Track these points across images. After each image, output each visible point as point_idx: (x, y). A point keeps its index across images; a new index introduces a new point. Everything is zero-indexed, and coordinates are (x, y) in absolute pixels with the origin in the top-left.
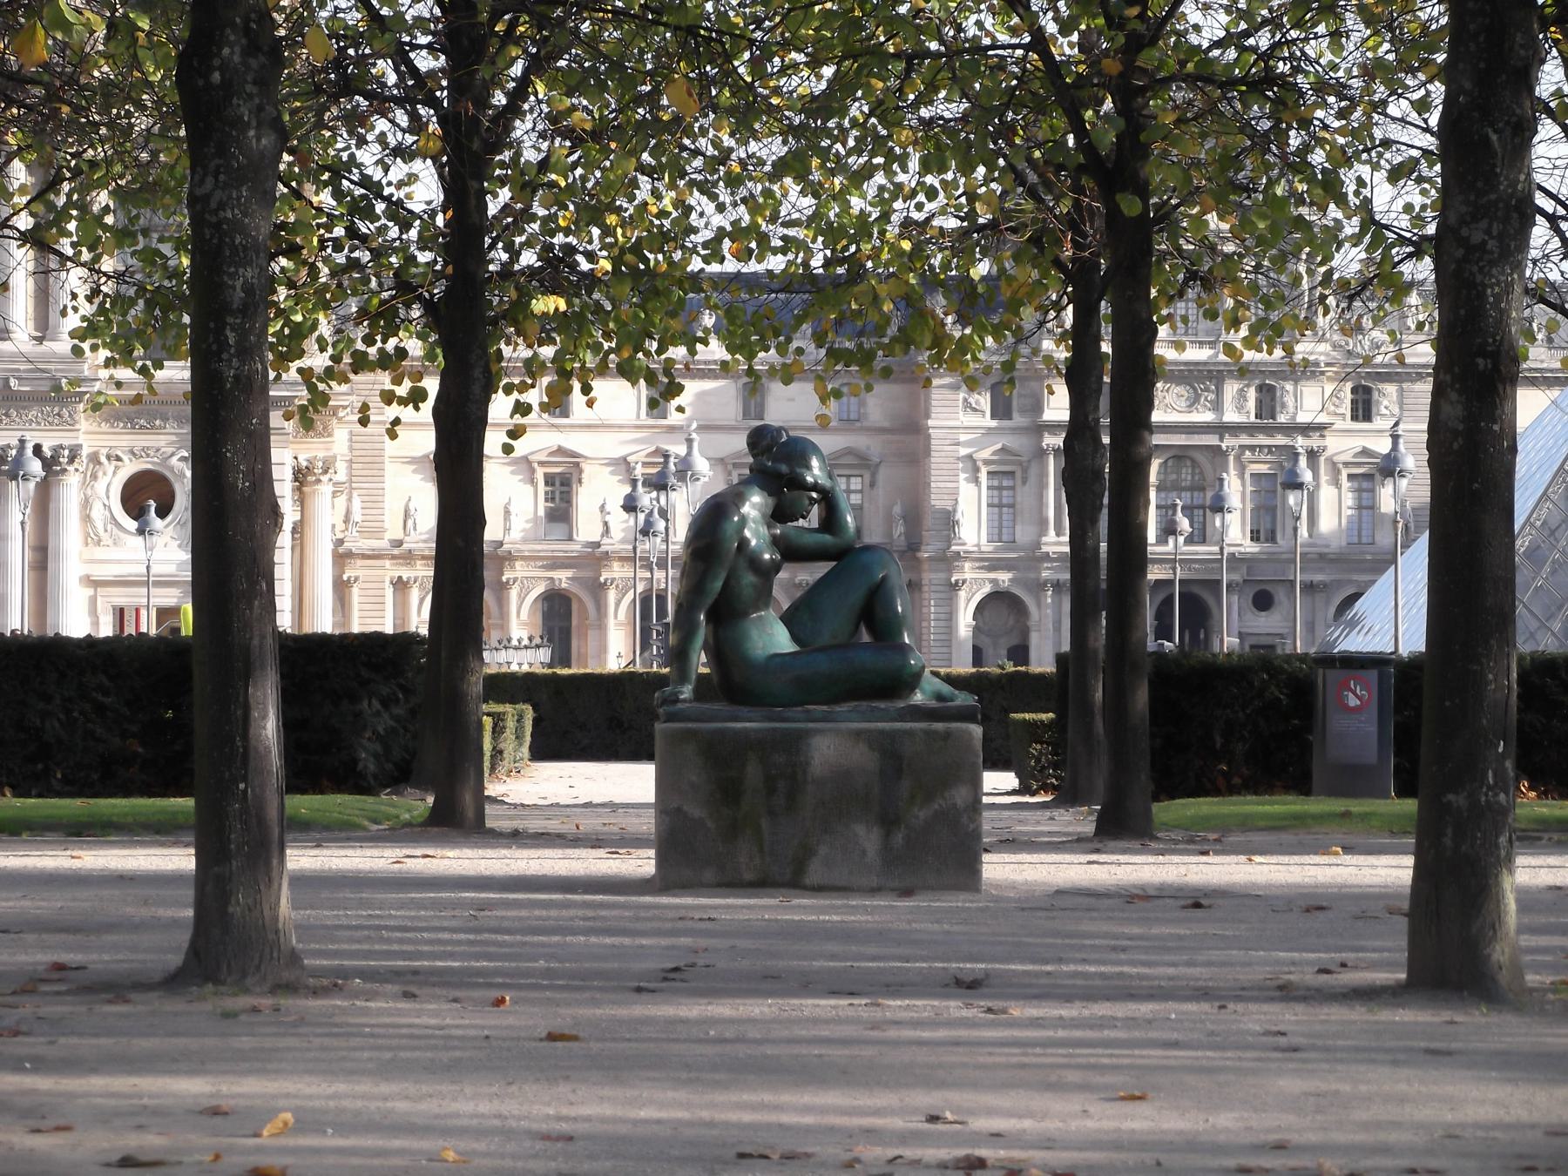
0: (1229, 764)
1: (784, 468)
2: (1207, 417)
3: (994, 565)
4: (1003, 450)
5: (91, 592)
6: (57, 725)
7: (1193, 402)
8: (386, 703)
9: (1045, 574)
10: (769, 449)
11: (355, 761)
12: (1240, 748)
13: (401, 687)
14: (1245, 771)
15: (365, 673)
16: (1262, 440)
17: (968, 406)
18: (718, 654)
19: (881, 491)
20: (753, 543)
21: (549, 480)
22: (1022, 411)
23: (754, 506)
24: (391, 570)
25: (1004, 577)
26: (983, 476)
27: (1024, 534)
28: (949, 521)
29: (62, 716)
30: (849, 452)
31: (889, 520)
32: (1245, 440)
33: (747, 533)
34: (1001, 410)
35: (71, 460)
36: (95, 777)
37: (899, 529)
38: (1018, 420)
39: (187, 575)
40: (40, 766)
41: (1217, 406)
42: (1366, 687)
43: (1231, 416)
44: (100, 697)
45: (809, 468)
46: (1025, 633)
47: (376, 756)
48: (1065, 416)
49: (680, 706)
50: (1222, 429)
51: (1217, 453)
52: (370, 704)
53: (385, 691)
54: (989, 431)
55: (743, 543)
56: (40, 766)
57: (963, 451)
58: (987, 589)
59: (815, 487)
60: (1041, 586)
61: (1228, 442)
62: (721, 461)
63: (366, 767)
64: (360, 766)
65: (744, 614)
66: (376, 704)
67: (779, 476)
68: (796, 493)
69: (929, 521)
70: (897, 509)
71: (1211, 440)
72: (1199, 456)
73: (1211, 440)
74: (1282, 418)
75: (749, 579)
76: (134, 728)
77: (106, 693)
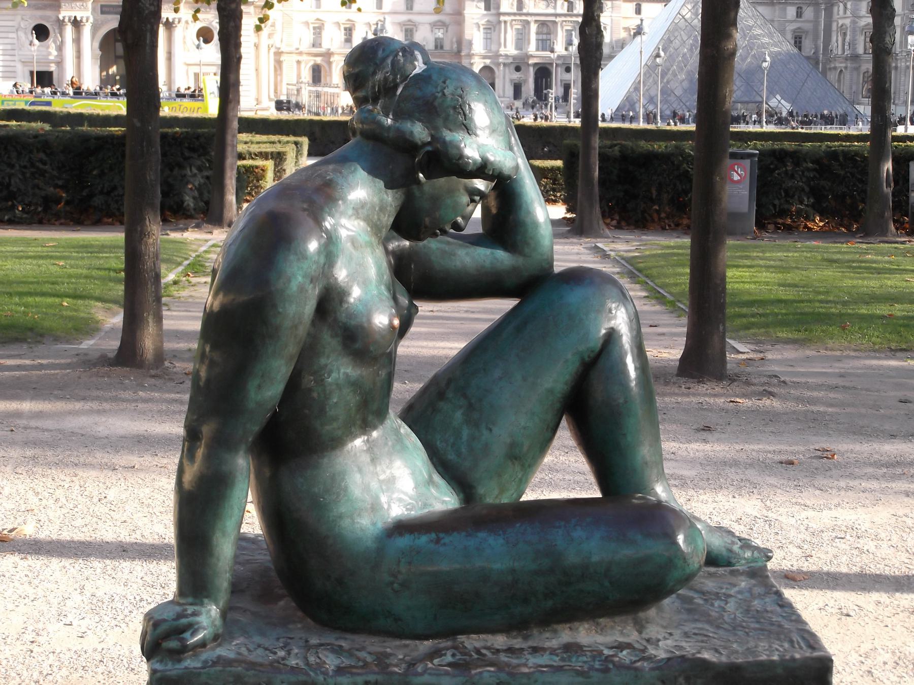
0: (659, 206)
1: (419, 131)
2: (550, 11)
3: (485, 57)
4: (488, 21)
5: (186, 67)
6: (18, 181)
7: (548, 6)
8: (200, 169)
9: (501, 60)
10: (388, 89)
11: (183, 202)
12: (665, 197)
13: (208, 160)
14: (667, 209)
15: (187, 154)
16: (569, 19)
17: (477, 6)
18: (276, 514)
19: (450, 34)
20: (356, 293)
21: (345, 29)
22: (494, 8)
23: (359, 210)
24: (296, 58)
25: (488, 62)
26: (482, 27)
27: (494, 48)
28: (470, 43)
29: (20, 176)
30: (440, 21)
31: (452, 43)
32: (563, 19)
33: (341, 274)
34: (487, 8)
35: (179, 22)
36: (40, 209)
37: (455, 46)
38: (493, 11)
39: (219, 62)
40: (10, 203)
41: (555, 8)
42: (744, 170)
43: (559, 11)
44: (41, 166)
45: (468, 128)
46: (494, 79)
47: (194, 198)
48: (582, 12)
49: (190, 662)
50: (556, 15)
51: (555, 22)
52: (191, 170)
53: (199, 163)
54: (484, 15)
55: (330, 301)
56: (10, 203)
57: (475, 21)
58: (482, 65)
59: (483, 170)
60: (498, 64)
61: (558, 19)
62: (399, 24)
63: (188, 205)
64: (185, 204)
65: (337, 443)
66: (195, 171)
67: (408, 147)
68: (442, 181)
69: (464, 44)
70: (454, 40)
71: (553, 18)
72: (549, 24)
73: (553, 18)
74: (525, 11)
75: (340, 370)
76: (60, 183)
77: (45, 164)
